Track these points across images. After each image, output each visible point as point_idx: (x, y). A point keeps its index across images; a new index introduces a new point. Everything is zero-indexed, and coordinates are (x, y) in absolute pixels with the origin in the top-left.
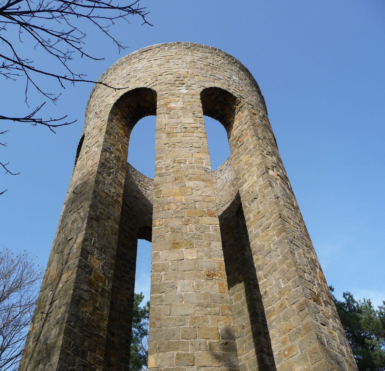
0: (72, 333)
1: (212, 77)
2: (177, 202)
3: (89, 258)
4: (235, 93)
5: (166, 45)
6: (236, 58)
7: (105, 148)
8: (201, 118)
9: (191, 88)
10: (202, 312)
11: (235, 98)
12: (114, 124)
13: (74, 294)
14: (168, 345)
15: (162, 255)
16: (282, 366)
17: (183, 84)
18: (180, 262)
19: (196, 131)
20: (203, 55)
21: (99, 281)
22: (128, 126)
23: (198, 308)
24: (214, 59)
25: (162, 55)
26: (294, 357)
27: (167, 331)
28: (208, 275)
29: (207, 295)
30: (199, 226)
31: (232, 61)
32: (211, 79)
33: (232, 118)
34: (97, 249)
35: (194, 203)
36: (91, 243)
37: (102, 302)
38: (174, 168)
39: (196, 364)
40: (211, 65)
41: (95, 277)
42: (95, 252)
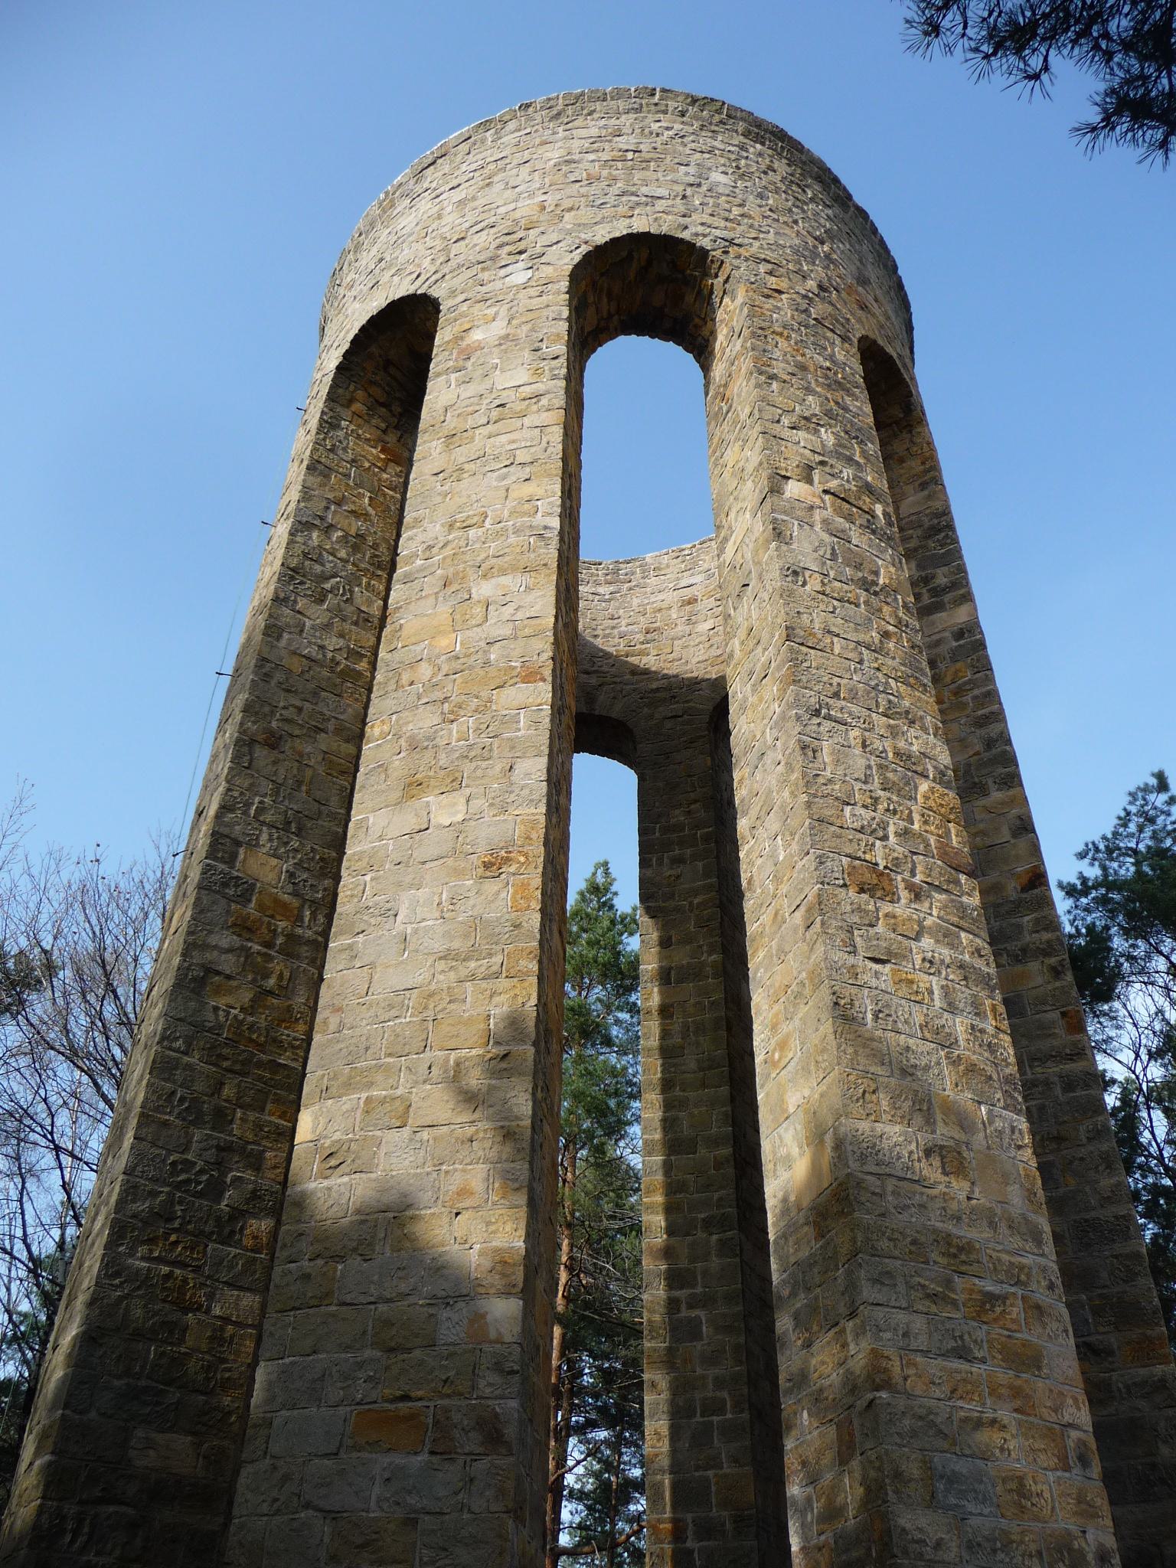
0: (176, 1068)
1: (624, 199)
2: (438, 657)
3: (241, 857)
4: (705, 236)
5: (486, 125)
6: (731, 100)
7: (304, 519)
8: (556, 358)
9: (543, 259)
10: (452, 975)
11: (704, 253)
12: (341, 434)
13: (186, 964)
14: (350, 1078)
15: (374, 824)
16: (767, 1094)
17: (520, 253)
18: (417, 837)
19: (535, 408)
20: (605, 127)
21: (278, 917)
22: (396, 427)
23: (441, 965)
24: (647, 131)
25: (474, 167)
26: (789, 1067)
27: (354, 1040)
28: (487, 866)
29: (477, 923)
30: (487, 717)
31: (717, 118)
32: (619, 209)
33: (710, 323)
34: (271, 826)
35: (487, 648)
36: (245, 813)
37: (287, 974)
38: (449, 548)
39: (410, 1121)
40: (630, 155)
41: (261, 907)
42: (264, 837)
